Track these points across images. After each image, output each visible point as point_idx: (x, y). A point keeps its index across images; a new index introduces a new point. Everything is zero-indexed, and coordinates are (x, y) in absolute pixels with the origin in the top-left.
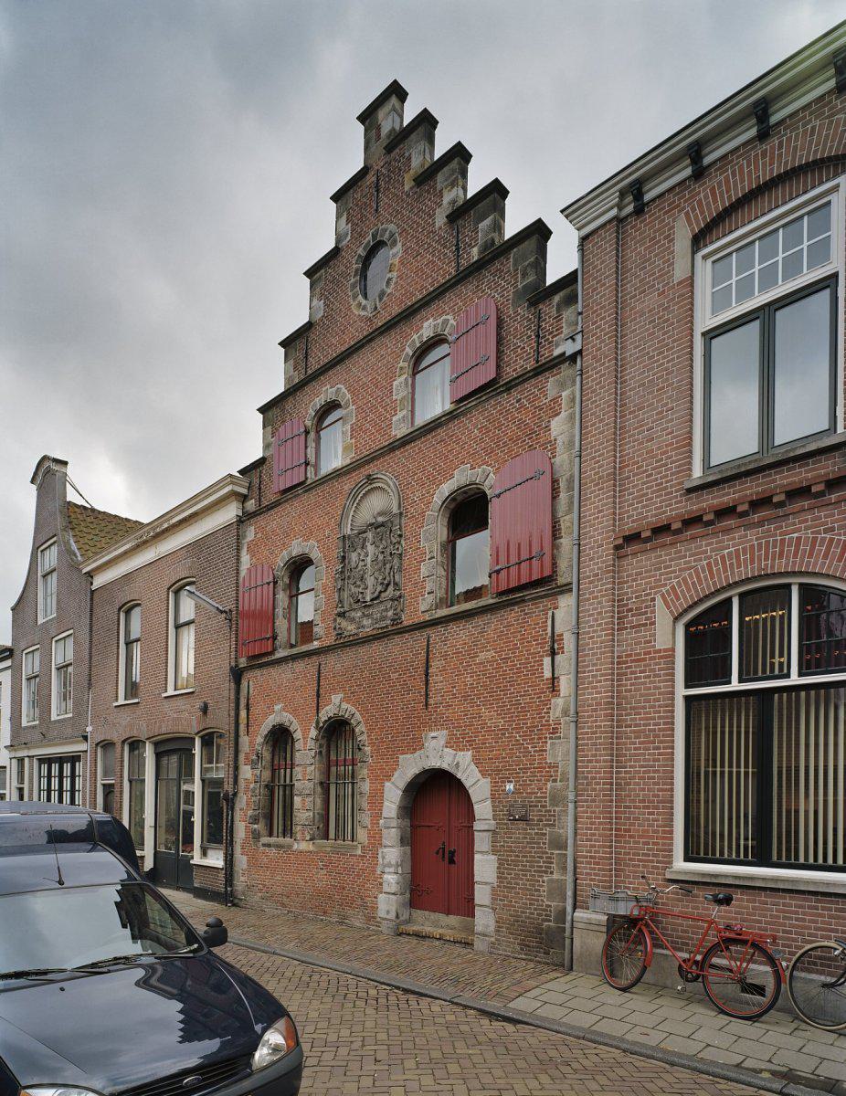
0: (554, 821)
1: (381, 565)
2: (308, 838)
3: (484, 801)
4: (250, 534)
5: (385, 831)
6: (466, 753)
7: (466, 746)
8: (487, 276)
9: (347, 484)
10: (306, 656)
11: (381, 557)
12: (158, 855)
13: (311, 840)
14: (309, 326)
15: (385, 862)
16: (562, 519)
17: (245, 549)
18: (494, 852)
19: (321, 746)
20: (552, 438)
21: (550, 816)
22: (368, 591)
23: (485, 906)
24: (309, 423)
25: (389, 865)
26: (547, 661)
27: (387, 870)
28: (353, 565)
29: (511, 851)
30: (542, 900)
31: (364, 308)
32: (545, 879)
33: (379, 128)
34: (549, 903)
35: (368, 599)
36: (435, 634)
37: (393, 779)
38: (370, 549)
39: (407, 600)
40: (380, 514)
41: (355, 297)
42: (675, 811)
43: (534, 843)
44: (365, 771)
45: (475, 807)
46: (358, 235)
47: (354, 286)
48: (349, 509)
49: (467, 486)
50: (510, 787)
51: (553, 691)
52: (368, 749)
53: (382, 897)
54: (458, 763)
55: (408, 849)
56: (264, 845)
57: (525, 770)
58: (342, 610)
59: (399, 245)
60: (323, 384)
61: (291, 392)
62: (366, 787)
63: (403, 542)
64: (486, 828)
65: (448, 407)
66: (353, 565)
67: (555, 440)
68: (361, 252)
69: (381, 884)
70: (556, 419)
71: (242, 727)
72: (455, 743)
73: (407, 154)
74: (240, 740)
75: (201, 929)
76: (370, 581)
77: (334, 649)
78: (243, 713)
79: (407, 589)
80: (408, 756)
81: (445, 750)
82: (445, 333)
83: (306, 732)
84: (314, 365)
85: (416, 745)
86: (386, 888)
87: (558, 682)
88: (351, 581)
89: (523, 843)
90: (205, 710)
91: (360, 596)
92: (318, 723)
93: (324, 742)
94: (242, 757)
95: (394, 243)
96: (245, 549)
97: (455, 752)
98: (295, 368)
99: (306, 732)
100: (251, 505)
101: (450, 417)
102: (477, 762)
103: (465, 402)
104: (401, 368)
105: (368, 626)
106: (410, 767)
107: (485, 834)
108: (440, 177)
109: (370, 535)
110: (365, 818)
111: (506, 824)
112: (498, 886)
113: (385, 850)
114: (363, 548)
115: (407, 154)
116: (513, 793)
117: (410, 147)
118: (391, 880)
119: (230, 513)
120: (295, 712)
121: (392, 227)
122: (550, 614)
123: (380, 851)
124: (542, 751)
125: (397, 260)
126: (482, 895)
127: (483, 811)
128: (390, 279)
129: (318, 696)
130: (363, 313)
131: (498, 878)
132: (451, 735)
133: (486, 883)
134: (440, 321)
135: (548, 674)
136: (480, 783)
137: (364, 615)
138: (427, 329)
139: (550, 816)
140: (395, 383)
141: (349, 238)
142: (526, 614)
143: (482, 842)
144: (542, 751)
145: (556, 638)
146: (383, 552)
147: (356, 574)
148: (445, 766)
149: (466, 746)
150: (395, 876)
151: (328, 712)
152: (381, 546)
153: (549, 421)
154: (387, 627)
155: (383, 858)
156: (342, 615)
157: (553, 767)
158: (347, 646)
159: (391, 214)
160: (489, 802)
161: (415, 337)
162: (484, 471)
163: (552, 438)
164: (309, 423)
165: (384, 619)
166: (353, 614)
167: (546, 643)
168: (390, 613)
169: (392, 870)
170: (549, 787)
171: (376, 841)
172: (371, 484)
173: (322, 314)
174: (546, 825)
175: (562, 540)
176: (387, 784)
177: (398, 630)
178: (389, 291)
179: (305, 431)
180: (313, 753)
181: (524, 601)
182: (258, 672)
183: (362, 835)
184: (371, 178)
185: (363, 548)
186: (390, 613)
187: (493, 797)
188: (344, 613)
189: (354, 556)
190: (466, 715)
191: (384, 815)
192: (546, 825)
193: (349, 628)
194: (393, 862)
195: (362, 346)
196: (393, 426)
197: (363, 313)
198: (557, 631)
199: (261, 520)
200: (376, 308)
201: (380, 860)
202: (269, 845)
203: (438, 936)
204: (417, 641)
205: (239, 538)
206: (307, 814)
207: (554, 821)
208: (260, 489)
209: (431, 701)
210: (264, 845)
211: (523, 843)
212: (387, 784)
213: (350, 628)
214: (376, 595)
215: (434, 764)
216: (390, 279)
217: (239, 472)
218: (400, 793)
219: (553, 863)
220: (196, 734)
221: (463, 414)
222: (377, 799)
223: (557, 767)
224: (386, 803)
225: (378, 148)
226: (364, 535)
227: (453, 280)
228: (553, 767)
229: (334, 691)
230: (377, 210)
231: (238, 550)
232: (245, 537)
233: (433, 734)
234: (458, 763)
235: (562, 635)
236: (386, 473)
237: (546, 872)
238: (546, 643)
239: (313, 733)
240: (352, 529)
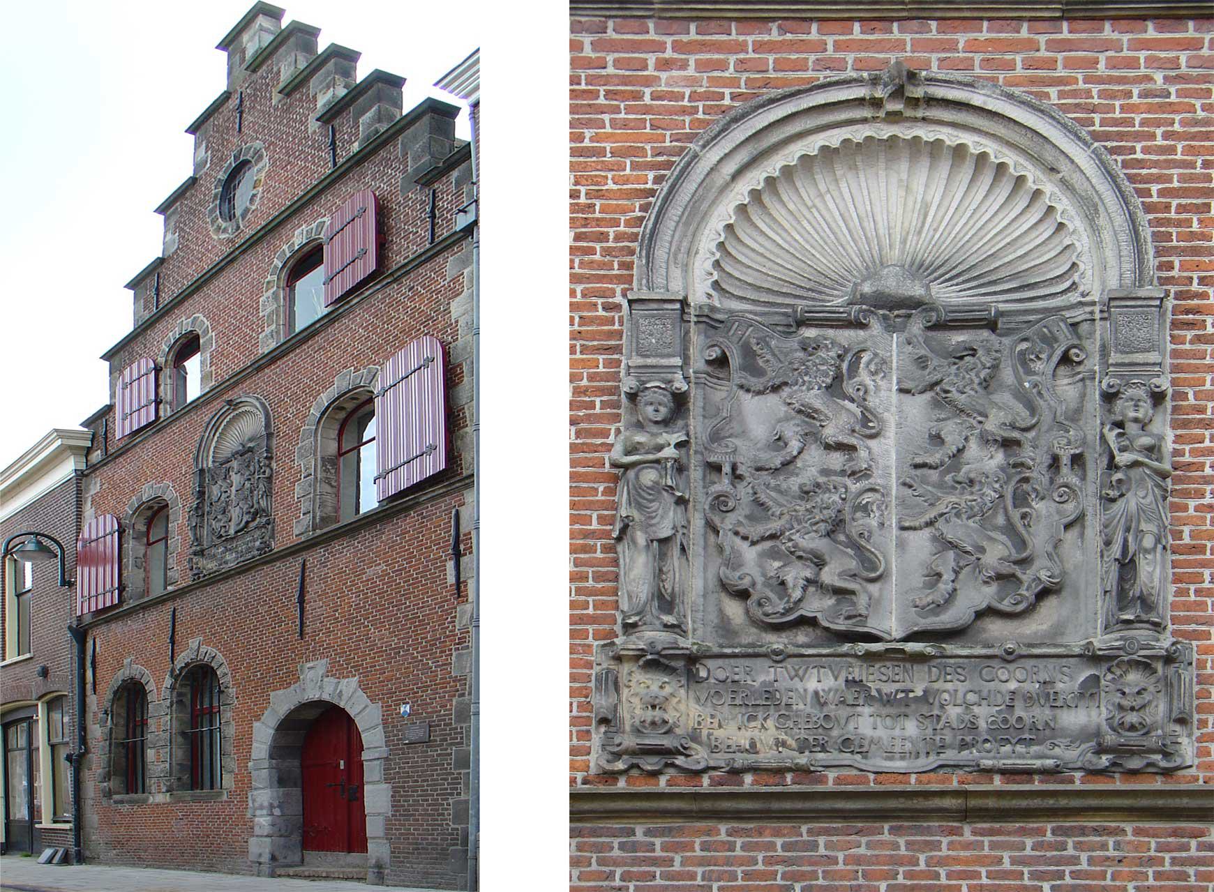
0: (462, 738)
1: (246, 494)
2: (164, 790)
3: (374, 727)
4: (95, 487)
5: (254, 773)
6: (351, 679)
7: (351, 672)
8: (370, 168)
9: (206, 415)
10: (158, 603)
11: (248, 485)
12: (14, 830)
13: (167, 791)
14: (160, 262)
15: (256, 805)
16: (466, 407)
17: (89, 504)
18: (387, 780)
19: (179, 695)
20: (453, 321)
21: (455, 733)
22: (232, 524)
23: (379, 838)
24: (161, 360)
25: (261, 808)
26: (450, 565)
27: (258, 812)
28: (215, 498)
29: (408, 777)
30: (447, 824)
31: (225, 231)
32: (451, 801)
33: (243, 51)
34: (456, 826)
35: (232, 532)
36: (313, 558)
37: (263, 718)
38: (236, 479)
39: (279, 525)
40: (250, 440)
41: (213, 222)
42: (234, 876)
43: (437, 765)
44: (229, 714)
45: (362, 736)
46: (218, 160)
47: (212, 211)
48: (209, 440)
49: (350, 391)
50: (405, 709)
51: (459, 597)
52: (232, 691)
53: (252, 841)
54: (341, 691)
55: (296, 792)
56: (116, 802)
57: (425, 688)
58: (198, 548)
59: (266, 159)
60: (179, 317)
61: (142, 330)
62: (231, 731)
63: (274, 465)
64: (377, 755)
65: (322, 311)
66: (215, 498)
67: (457, 322)
68: (222, 176)
69: (252, 828)
70: (457, 299)
71: (89, 687)
72: (337, 671)
73: (275, 69)
74: (88, 700)
75: (603, 729)
76: (235, 513)
77: (191, 591)
78: (89, 674)
79: (279, 514)
80: (280, 692)
81: (325, 679)
82: (321, 236)
83: (159, 682)
84: (166, 298)
85: (290, 678)
86: (257, 831)
87: (465, 586)
88: (213, 516)
89: (423, 766)
90: (45, 673)
91: (223, 530)
92: (173, 671)
93: (187, 690)
94: (90, 716)
95: (261, 157)
96: (89, 504)
97: (336, 680)
98: (145, 308)
99: (159, 682)
100: (96, 456)
101: (330, 320)
102: (364, 687)
103: (342, 303)
104: (268, 282)
105: (231, 560)
106: (282, 703)
107: (375, 762)
108: (313, 82)
109: (235, 464)
110: (231, 764)
111: (400, 749)
112: (393, 815)
113: (255, 793)
114: (225, 478)
115: (275, 69)
116: (409, 715)
117: (279, 61)
118: (263, 821)
119: (67, 469)
120: (146, 664)
121: (258, 144)
122: (454, 512)
123: (249, 794)
124: (445, 664)
125: (263, 174)
126: (374, 828)
127: (373, 739)
128: (254, 195)
129: (173, 642)
130: (223, 236)
131: (393, 806)
132: (333, 663)
133: (379, 814)
134: (314, 225)
135: (451, 579)
136: (368, 710)
137: (227, 550)
138: (298, 236)
139: (455, 733)
140: (261, 299)
141: (208, 165)
142: (424, 517)
143: (372, 772)
144: (445, 664)
145: (462, 537)
146: (249, 479)
147: (218, 507)
148: (326, 697)
149: (351, 672)
150: (268, 818)
151: (182, 659)
152: (247, 473)
153: (449, 303)
154: (254, 557)
155: (254, 801)
156: (201, 553)
157: (460, 680)
158: (206, 585)
159: (256, 132)
160: (381, 727)
161: (285, 247)
162: (369, 371)
163: (453, 321)
164: (161, 360)
165: (249, 550)
166: (213, 551)
167: (449, 545)
168: (257, 543)
169: (265, 812)
170: (454, 703)
171: (245, 784)
172: (234, 410)
173: (176, 247)
174: (452, 744)
175: (467, 429)
176: (256, 724)
177: (267, 558)
178: (254, 208)
179: (155, 369)
180: (168, 703)
181: (418, 504)
182: (104, 628)
183: (228, 781)
184: (233, 102)
185: (225, 478)
186: (257, 543)
187: (385, 723)
188: (202, 551)
189: (215, 490)
190: (351, 639)
191: (253, 757)
192: (452, 744)
193: (209, 566)
194: (266, 804)
195: (222, 269)
196: (260, 344)
197: (223, 236)
198: (463, 530)
199: (107, 471)
200: (238, 227)
201: (251, 804)
202: (122, 802)
203: (324, 875)
204: (292, 567)
205: (79, 492)
206: (163, 766)
207: (462, 738)
208: (106, 438)
209: (308, 630)
210: (116, 802)
211: (423, 766)
212: (256, 724)
213: (211, 565)
214: (242, 525)
215: (313, 695)
216: (254, 195)
217: (83, 424)
218: (272, 732)
219: (460, 783)
220: (39, 698)
221: (340, 316)
222: (245, 741)
223: (465, 679)
224: (254, 745)
225: (240, 72)
226: (228, 465)
227: (328, 181)
228: (460, 680)
229: (192, 635)
230: (240, 130)
231: (79, 504)
232: (87, 491)
233: (311, 664)
234: (341, 691)
235: (470, 533)
236: (250, 397)
237: (452, 794)
238: (449, 545)
239: (168, 682)
240: (214, 462)
